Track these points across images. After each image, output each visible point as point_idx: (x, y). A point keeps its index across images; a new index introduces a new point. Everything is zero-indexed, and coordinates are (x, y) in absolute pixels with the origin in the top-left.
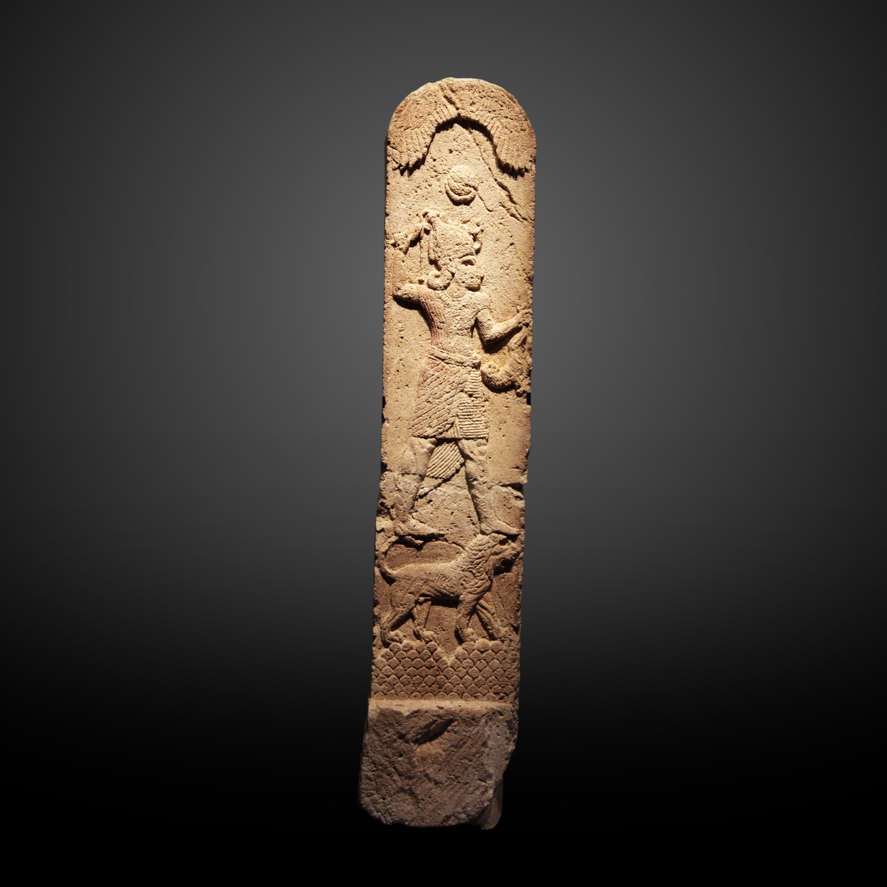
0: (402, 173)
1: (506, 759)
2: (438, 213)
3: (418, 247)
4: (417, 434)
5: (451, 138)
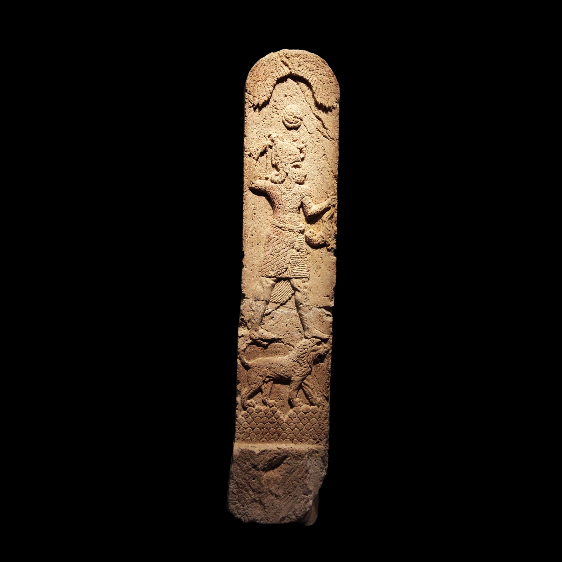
0: (255, 110)
1: (321, 481)
2: (278, 135)
3: (265, 156)
4: (264, 275)
5: (286, 88)
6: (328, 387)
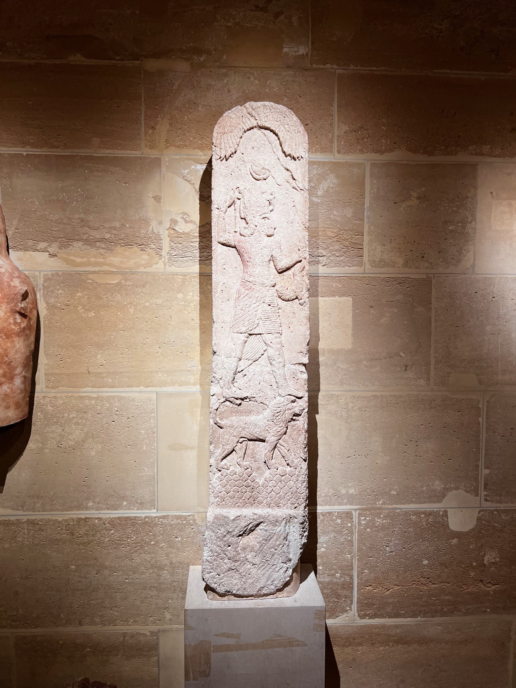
1: (301, 549)
4: (235, 331)
6: (305, 448)
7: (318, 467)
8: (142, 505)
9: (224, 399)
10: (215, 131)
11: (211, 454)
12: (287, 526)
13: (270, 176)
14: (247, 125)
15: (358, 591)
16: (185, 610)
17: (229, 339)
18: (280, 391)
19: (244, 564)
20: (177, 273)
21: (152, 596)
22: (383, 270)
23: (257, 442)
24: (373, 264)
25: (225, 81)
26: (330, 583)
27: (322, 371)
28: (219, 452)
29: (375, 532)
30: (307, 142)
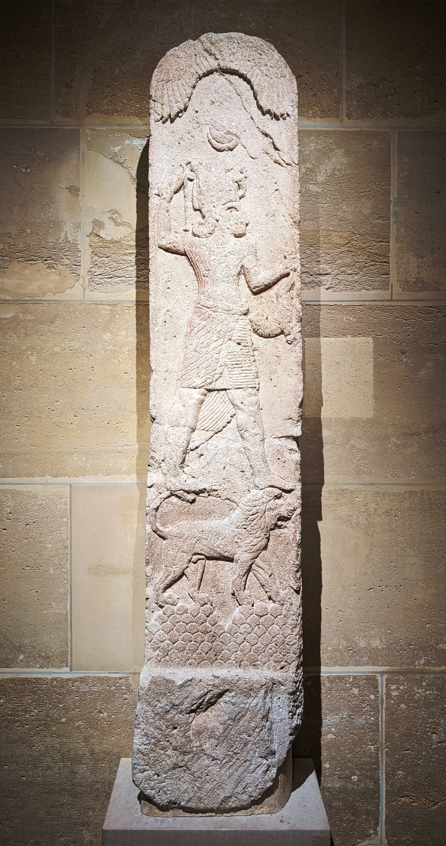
1: (291, 735)
4: (185, 384)
6: (297, 571)
7: (323, 605)
8: (47, 660)
9: (168, 493)
10: (154, 78)
11: (149, 579)
12: (268, 698)
13: (239, 145)
14: (202, 67)
15: (387, 804)
16: (104, 831)
17: (176, 398)
18: (257, 481)
19: (199, 758)
20: (102, 301)
21: (62, 805)
22: (421, 295)
23: (220, 562)
24: (406, 285)
25: (176, 15)
26: (343, 790)
27: (328, 452)
28: (160, 578)
29: (413, 709)
30: (297, 92)
